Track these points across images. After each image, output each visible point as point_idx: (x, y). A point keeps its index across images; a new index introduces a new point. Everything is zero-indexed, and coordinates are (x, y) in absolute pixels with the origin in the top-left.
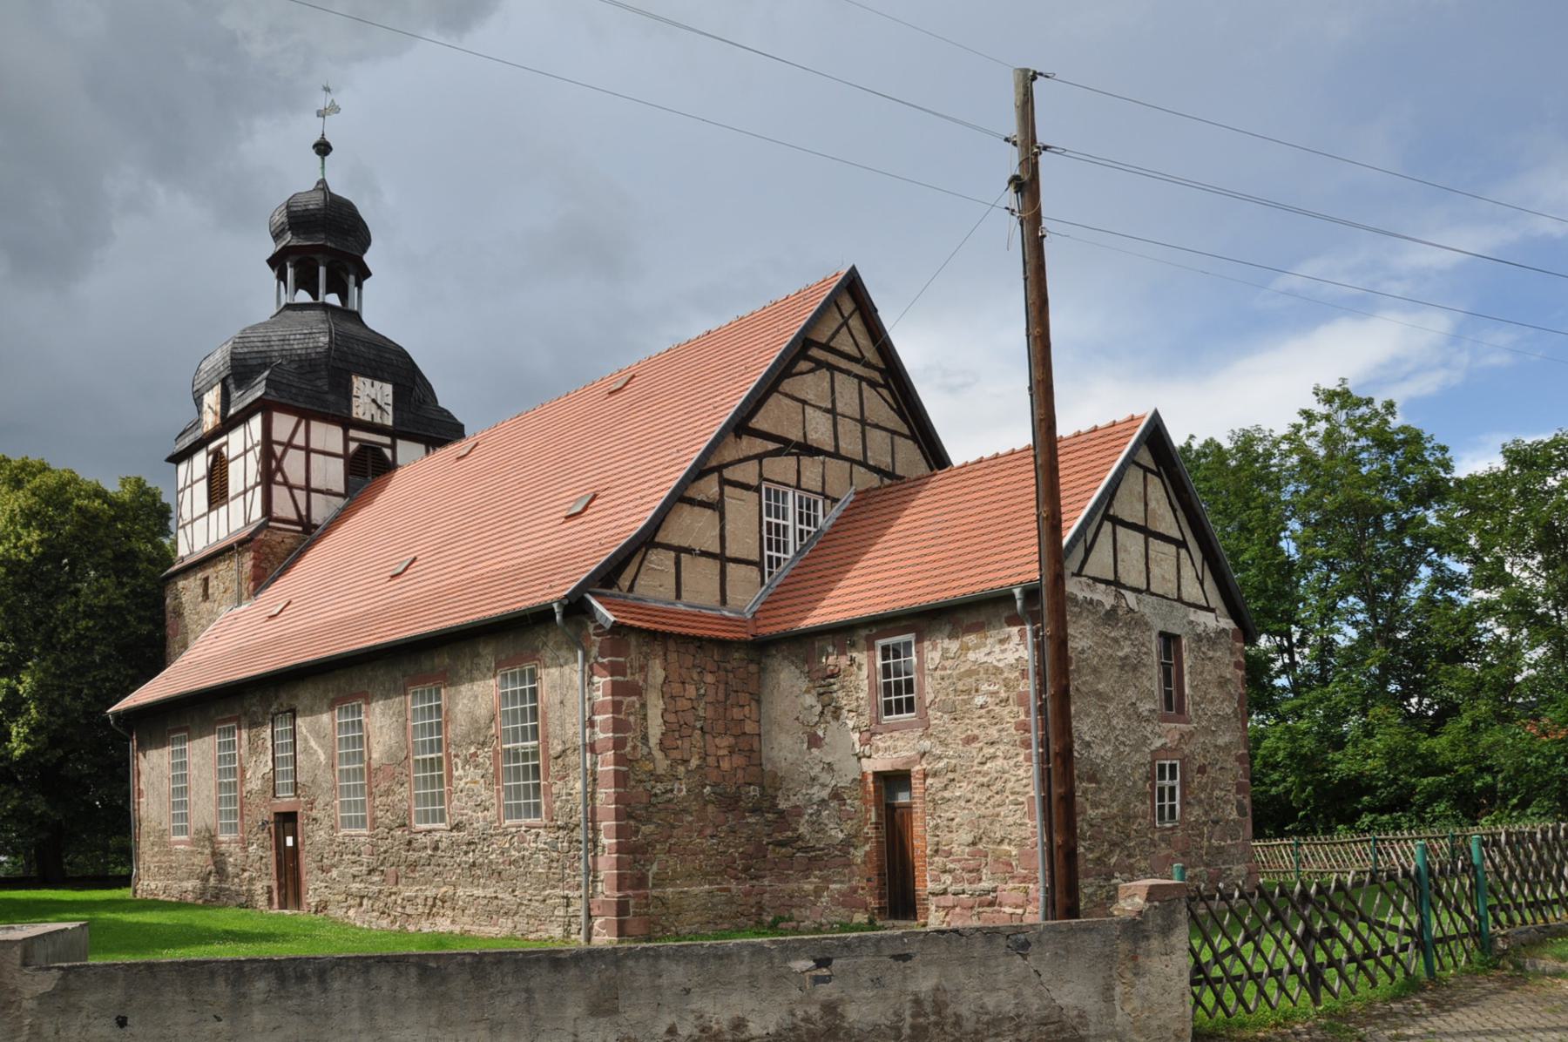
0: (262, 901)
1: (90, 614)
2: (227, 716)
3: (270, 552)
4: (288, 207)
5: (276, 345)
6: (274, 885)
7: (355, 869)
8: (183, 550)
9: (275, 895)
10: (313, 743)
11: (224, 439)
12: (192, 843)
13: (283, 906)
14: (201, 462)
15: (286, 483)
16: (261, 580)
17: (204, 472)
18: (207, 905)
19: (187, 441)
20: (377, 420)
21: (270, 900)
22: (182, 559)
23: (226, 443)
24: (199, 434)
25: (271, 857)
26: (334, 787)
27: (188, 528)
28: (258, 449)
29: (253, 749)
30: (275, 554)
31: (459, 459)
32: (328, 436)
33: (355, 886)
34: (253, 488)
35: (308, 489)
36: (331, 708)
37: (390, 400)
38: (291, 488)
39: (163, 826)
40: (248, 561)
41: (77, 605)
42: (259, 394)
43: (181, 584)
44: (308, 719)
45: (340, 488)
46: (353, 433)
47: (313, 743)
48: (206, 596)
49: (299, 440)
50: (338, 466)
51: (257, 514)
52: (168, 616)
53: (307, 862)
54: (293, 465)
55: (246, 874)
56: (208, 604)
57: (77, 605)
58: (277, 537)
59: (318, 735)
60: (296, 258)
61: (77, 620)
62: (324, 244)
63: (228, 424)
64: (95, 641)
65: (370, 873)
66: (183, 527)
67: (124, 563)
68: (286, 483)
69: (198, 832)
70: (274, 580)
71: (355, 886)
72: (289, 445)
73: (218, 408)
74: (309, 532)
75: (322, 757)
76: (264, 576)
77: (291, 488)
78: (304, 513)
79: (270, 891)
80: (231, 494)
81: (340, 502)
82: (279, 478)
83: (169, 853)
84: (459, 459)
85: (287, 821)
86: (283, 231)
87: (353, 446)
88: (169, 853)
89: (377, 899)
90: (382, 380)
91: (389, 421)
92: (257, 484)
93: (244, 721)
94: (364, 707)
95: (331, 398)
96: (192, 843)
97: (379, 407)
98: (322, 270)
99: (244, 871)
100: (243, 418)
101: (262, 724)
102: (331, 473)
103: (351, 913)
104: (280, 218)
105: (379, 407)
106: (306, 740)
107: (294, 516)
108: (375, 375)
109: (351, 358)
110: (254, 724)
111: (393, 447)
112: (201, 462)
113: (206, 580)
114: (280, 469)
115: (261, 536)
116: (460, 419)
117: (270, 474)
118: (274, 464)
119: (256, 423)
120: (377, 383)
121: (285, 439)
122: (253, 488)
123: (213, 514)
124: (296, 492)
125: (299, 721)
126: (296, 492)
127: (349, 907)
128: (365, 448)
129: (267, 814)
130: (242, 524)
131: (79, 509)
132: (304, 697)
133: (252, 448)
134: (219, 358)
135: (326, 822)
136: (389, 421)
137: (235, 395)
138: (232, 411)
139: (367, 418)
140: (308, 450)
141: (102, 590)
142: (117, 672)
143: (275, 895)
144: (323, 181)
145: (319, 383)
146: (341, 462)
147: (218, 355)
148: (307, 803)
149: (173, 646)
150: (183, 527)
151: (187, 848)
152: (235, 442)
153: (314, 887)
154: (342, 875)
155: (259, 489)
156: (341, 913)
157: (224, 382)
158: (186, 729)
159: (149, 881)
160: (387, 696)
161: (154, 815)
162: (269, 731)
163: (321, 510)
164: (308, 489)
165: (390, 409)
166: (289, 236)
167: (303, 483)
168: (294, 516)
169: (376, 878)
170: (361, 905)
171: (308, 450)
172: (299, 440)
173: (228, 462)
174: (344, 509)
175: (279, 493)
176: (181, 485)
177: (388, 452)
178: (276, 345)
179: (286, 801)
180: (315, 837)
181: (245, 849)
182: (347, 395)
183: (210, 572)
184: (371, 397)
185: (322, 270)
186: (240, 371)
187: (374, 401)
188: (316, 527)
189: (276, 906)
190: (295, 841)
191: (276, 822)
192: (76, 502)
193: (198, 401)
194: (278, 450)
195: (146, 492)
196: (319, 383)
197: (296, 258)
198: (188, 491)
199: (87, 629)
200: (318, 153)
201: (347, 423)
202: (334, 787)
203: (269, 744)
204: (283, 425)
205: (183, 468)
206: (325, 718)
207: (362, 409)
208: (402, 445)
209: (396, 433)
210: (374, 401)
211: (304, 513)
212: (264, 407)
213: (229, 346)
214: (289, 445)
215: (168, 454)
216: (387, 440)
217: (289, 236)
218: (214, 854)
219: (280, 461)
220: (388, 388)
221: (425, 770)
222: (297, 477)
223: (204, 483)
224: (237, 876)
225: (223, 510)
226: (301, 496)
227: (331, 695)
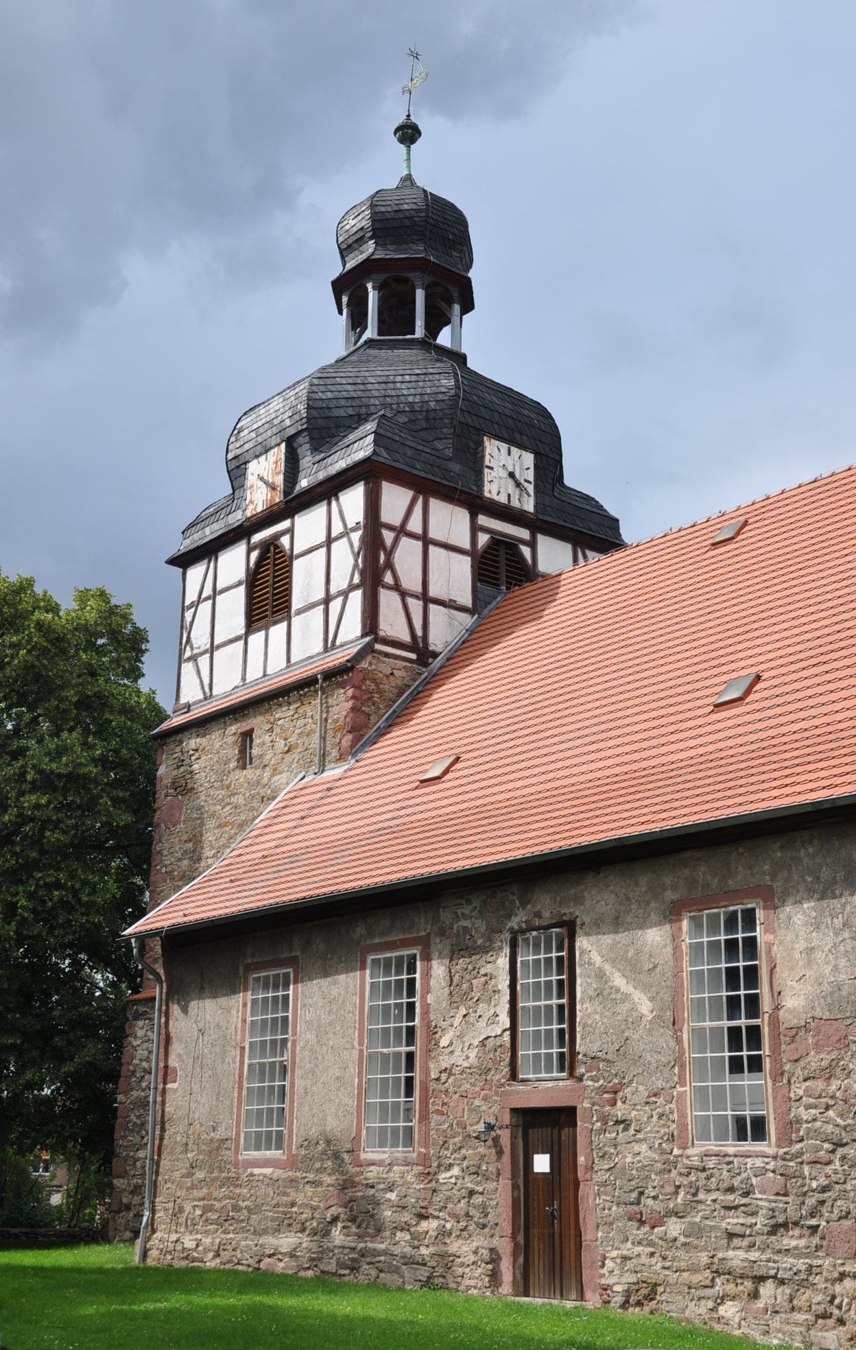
0: (473, 1278)
1: (47, 782)
2: (396, 937)
3: (377, 690)
4: (372, 206)
5: (376, 390)
6: (505, 1247)
7: (733, 1221)
8: (191, 692)
9: (506, 1267)
10: (619, 981)
11: (285, 524)
12: (292, 1163)
13: (524, 1286)
14: (234, 563)
15: (397, 587)
16: (363, 732)
17: (241, 575)
18: (326, 1282)
19: (210, 532)
20: (515, 503)
21: (495, 1277)
22: (188, 707)
23: (291, 531)
24: (236, 518)
25: (499, 1196)
26: (679, 1061)
27: (204, 661)
28: (356, 537)
29: (458, 994)
30: (381, 692)
31: (715, 545)
32: (450, 522)
33: (737, 1257)
34: (345, 594)
35: (426, 599)
36: (672, 914)
37: (530, 475)
38: (404, 594)
39: (221, 1133)
40: (341, 703)
41: (23, 774)
42: (360, 455)
43: (193, 743)
44: (607, 939)
45: (466, 599)
46: (483, 520)
47: (619, 981)
48: (244, 759)
49: (415, 525)
50: (463, 566)
51: (351, 628)
52: (161, 794)
53: (597, 1204)
54: (407, 556)
55: (430, 1226)
56: (249, 773)
57: (23, 774)
58: (385, 667)
59: (632, 968)
60: (383, 277)
61: (22, 793)
62: (412, 264)
63: (294, 503)
64: (45, 824)
65: (774, 1230)
66: (194, 658)
67: (95, 711)
68: (397, 587)
69: (308, 1143)
70: (382, 733)
71: (737, 1257)
72: (401, 531)
73: (279, 480)
74: (427, 667)
75: (645, 1007)
76: (367, 726)
77: (404, 594)
78: (419, 633)
79: (494, 1258)
80: (297, 603)
81: (467, 620)
82: (388, 578)
83: (234, 1182)
84: (715, 545)
85: (547, 1125)
86: (360, 241)
87: (483, 539)
88: (234, 1182)
89: (805, 1284)
90: (521, 446)
91: (529, 506)
92: (352, 588)
93: (437, 944)
94: (760, 915)
95: (456, 467)
96: (292, 1163)
97: (518, 485)
98: (420, 295)
99: (422, 1217)
100: (329, 490)
101: (485, 950)
102: (454, 577)
103: (729, 1310)
104: (362, 221)
105: (518, 485)
106: (601, 975)
107: (406, 637)
108: (513, 439)
109: (483, 411)
110: (462, 948)
111: (532, 544)
112: (234, 563)
113: (247, 736)
114: (389, 565)
115: (364, 664)
116: (613, 510)
117: (374, 572)
118: (382, 558)
119: (353, 500)
120: (514, 449)
121: (334, 546)
122: (345, 594)
123: (257, 639)
124: (410, 601)
125: (582, 943)
126: (410, 601)
127: (722, 1299)
128: (501, 544)
129: (492, 1109)
130: (319, 647)
131: (39, 625)
132: (598, 898)
133: (346, 533)
134: (284, 410)
135: (655, 1129)
136: (529, 506)
137: (307, 461)
138: (304, 483)
139: (502, 499)
140: (426, 541)
141: (60, 752)
142: (72, 875)
143: (506, 1267)
144: (409, 178)
145: (439, 445)
146: (466, 562)
147: (276, 404)
148: (602, 1090)
149: (169, 848)
150: (194, 658)
151: (279, 1173)
152: (308, 527)
153: (614, 1255)
154: (695, 1231)
155: (356, 597)
156: (697, 1311)
157: (290, 441)
158: (292, 962)
159: (178, 1231)
160: (826, 892)
161: (200, 1113)
162: (503, 962)
163: (444, 630)
164: (426, 599)
165: (531, 488)
166: (370, 247)
167: (418, 589)
168: (406, 637)
169: (792, 1240)
170: (755, 1295)
171: (426, 541)
172: (415, 525)
173: (292, 558)
174: (471, 631)
175: (389, 601)
176: (191, 597)
177: (526, 551)
178: (376, 390)
179: (544, 1088)
180: (615, 1160)
181: (428, 1176)
182: (477, 466)
183: (257, 722)
184: (505, 469)
185: (420, 295)
186: (321, 424)
187: (512, 475)
188: (435, 655)
189: (506, 1289)
190: (529, 1163)
191: (513, 1127)
192: (37, 615)
193: (236, 471)
194: (388, 536)
195: (112, 611)
196: (439, 445)
197: (383, 277)
198: (205, 607)
199: (37, 806)
200: (401, 141)
201: (476, 504)
202: (679, 1061)
203: (503, 984)
204: (395, 500)
205: (196, 573)
206: (655, 936)
207: (495, 487)
208: (543, 542)
209: (538, 525)
210: (512, 475)
211: (419, 633)
212: (367, 473)
213: (303, 389)
214: (401, 531)
215: (172, 552)
216: (524, 534)
217: (370, 247)
218: (347, 1185)
219: (390, 554)
220: (529, 459)
221: (259, 1125)
222: (411, 581)
223: (242, 590)
224: (405, 1228)
225: (278, 632)
226: (415, 606)
227: (670, 895)
